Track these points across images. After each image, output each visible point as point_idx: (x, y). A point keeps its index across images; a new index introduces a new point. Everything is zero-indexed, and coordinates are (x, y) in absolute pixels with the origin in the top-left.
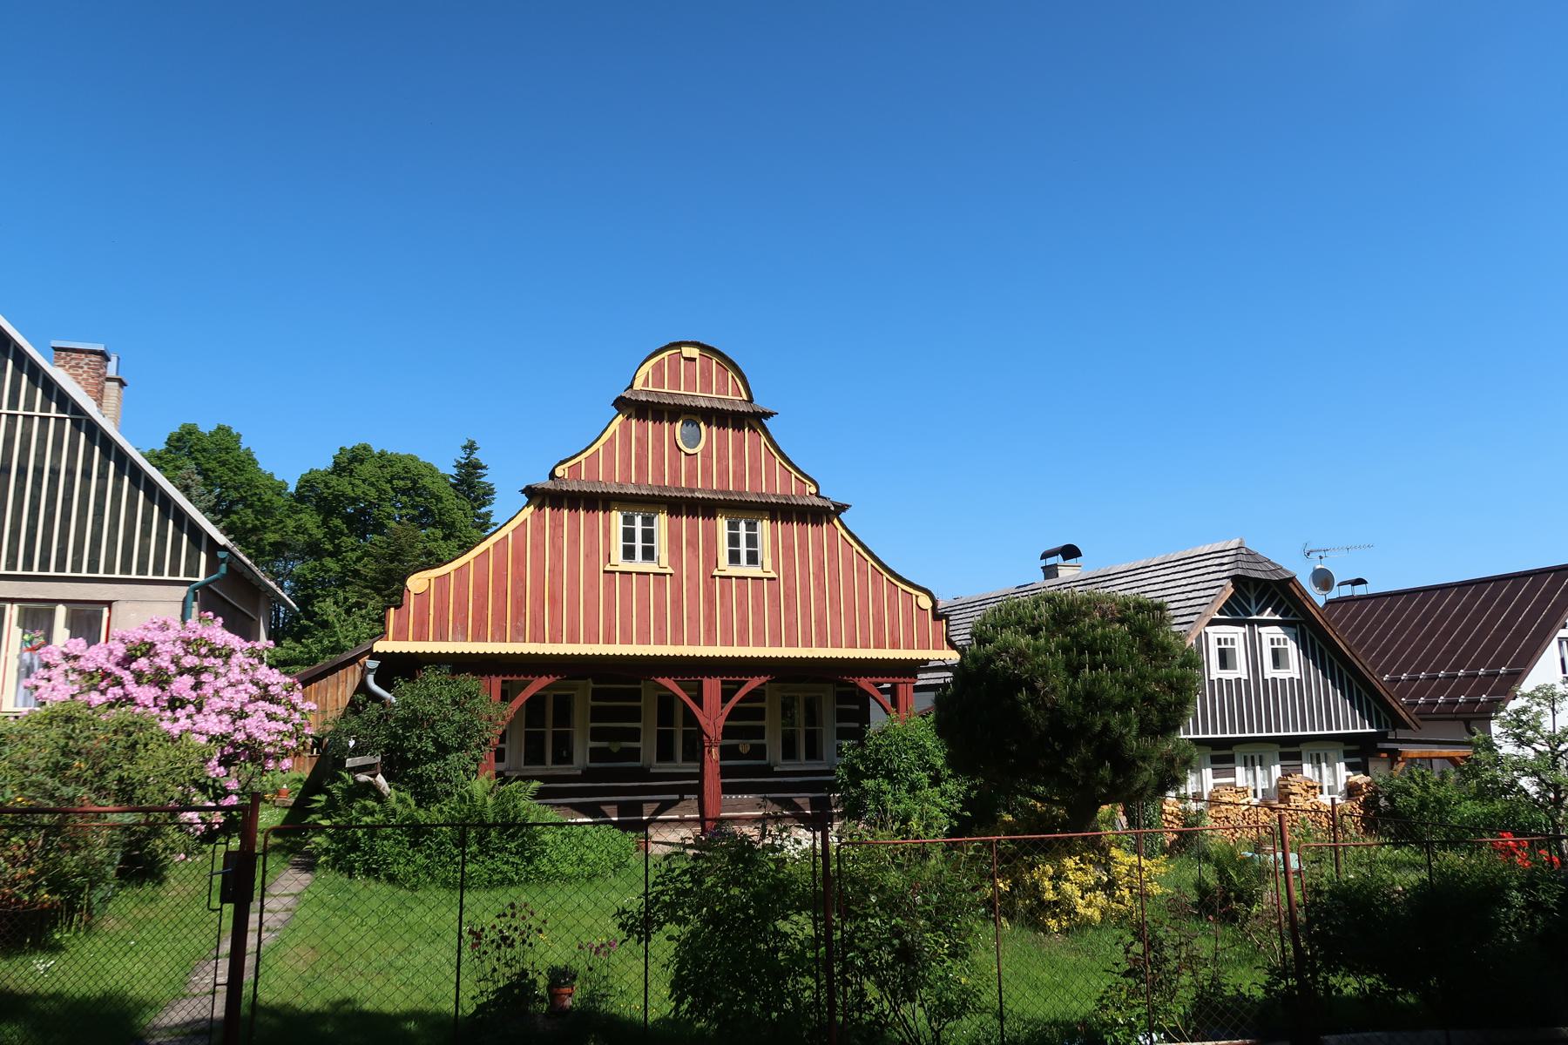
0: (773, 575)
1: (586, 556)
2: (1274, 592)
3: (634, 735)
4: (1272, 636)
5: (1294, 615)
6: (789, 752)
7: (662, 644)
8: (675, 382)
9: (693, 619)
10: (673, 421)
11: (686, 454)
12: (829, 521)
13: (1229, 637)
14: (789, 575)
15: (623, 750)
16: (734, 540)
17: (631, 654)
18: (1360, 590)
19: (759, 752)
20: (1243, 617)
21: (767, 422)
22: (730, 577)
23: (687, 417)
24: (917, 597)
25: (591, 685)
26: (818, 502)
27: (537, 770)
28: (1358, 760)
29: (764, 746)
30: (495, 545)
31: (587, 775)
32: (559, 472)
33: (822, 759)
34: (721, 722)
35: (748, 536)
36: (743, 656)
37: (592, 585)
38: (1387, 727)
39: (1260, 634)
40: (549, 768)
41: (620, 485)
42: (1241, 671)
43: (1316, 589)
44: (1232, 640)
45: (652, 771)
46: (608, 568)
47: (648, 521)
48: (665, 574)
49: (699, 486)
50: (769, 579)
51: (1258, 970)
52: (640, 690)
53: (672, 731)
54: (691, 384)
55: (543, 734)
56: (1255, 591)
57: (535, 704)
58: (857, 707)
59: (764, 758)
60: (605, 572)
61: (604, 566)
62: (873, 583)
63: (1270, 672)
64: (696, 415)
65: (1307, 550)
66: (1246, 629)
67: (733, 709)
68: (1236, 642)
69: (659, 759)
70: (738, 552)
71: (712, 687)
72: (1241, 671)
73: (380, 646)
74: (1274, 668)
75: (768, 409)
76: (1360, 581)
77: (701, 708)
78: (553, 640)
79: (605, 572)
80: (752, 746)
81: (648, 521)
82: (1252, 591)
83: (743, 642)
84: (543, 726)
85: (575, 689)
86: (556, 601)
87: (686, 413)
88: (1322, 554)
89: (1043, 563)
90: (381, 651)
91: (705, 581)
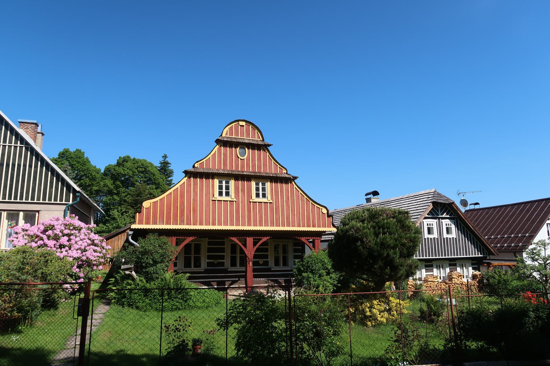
0: (271, 201)
1: (206, 195)
2: (447, 207)
3: (223, 257)
4: (446, 223)
5: (454, 216)
6: (277, 263)
7: (232, 226)
8: (237, 134)
9: (243, 217)
10: (236, 147)
11: (241, 159)
12: (291, 183)
13: (431, 223)
14: (277, 202)
15: (218, 263)
16: (257, 189)
17: (221, 229)
18: (477, 207)
19: (266, 263)
20: (436, 216)
21: (269, 148)
22: (256, 202)
23: (241, 146)
24: (322, 209)
25: (207, 240)
26: (287, 176)
27: (188, 270)
28: (477, 266)
29: (268, 261)
30: (174, 191)
31: (206, 271)
32: (196, 165)
33: (288, 266)
34: (253, 253)
35: (262, 188)
36: (261, 230)
37: (208, 205)
38: (486, 254)
39: (442, 222)
40: (193, 269)
41: (218, 170)
42: (435, 235)
43: (462, 206)
44: (432, 224)
45: (229, 270)
46: (213, 199)
47: (227, 182)
48: (233, 201)
49: (245, 170)
50: (270, 203)
51: (441, 340)
52: (224, 242)
53: (236, 256)
54: (242, 134)
55: (190, 257)
56: (440, 207)
57: (188, 247)
58: (301, 248)
59: (268, 266)
60: (212, 200)
61: (212, 198)
62: (306, 204)
63: (445, 235)
64: (244, 145)
65: (458, 193)
66: (437, 220)
67: (257, 248)
68: (434, 225)
69: (231, 266)
70: (259, 193)
71: (250, 241)
72: (435, 235)
73: (133, 226)
74: (447, 234)
75: (270, 143)
76: (477, 204)
77: (246, 248)
78: (194, 224)
79: (212, 200)
80: (264, 261)
81: (227, 182)
82: (439, 207)
83: (261, 225)
84: (191, 254)
85: (202, 241)
86: (195, 211)
87: (240, 145)
88: (464, 194)
89: (366, 197)
90: (134, 228)
91: (247, 204)
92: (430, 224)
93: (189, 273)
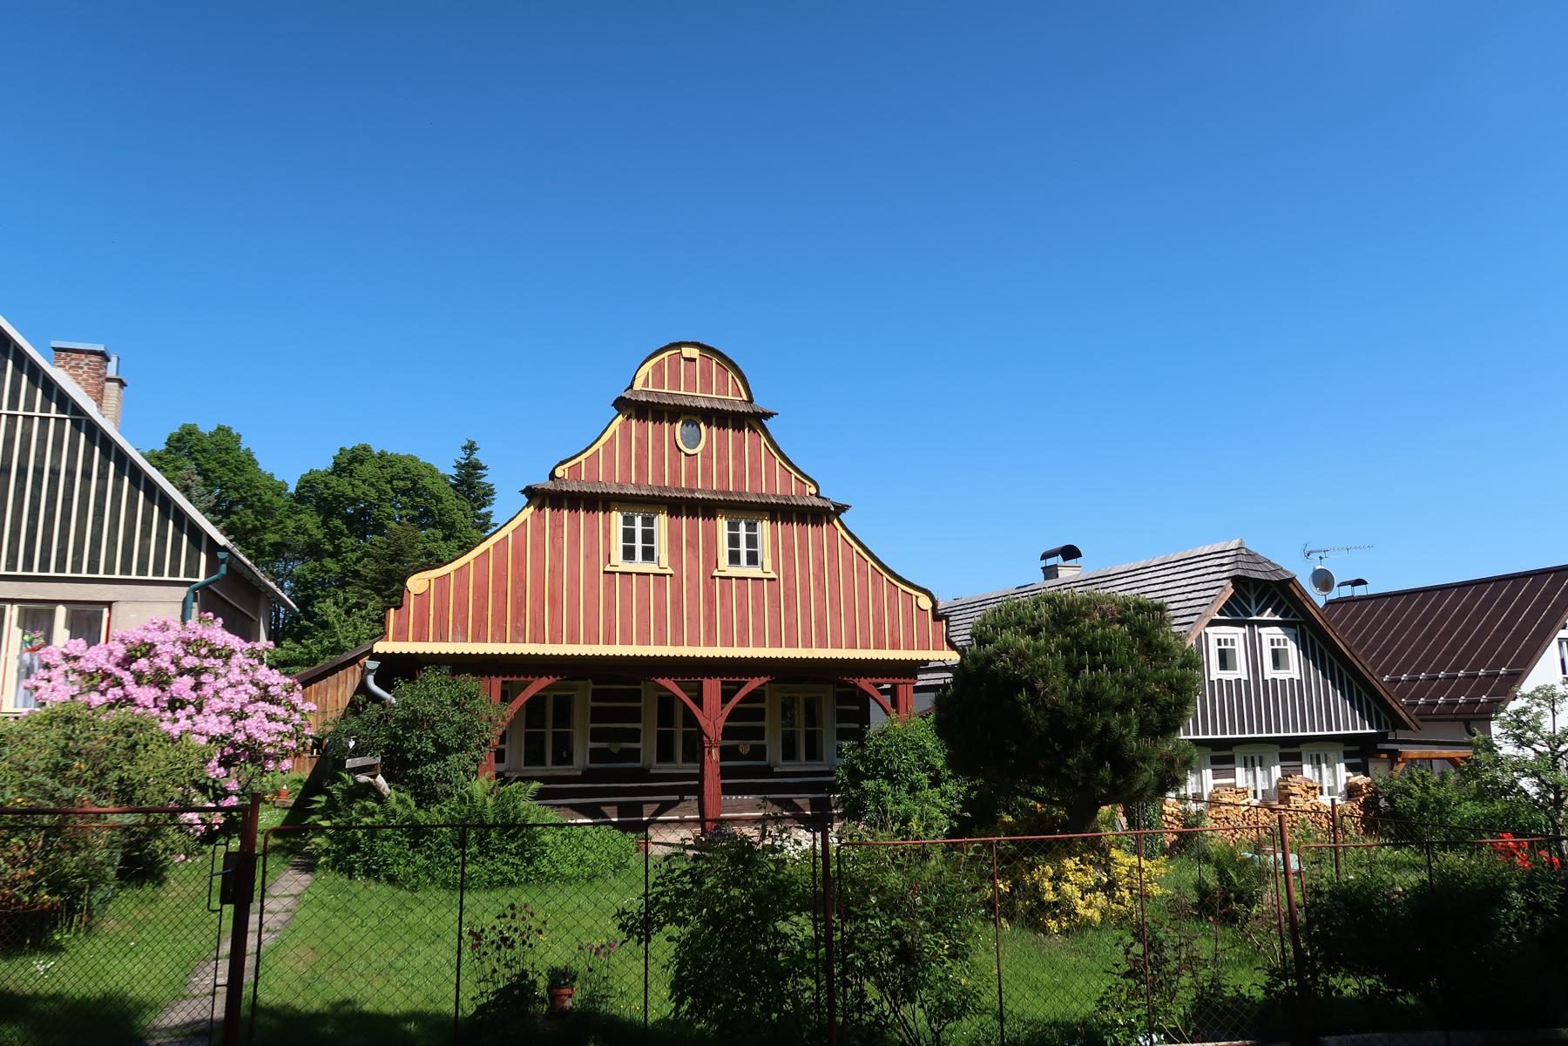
0: (773, 575)
1: (586, 557)
2: (1274, 592)
3: (634, 736)
4: (1272, 637)
5: (1294, 616)
6: (789, 753)
7: (662, 644)
8: (675, 383)
9: (693, 620)
10: (673, 421)
11: (686, 455)
12: (829, 522)
13: (1229, 637)
14: (789, 576)
15: (623, 750)
16: (734, 541)
17: (631, 655)
18: (1360, 591)
19: (759, 753)
20: (1243, 617)
21: (767, 423)
22: (730, 578)
23: (687, 417)
24: (917, 597)
25: (591, 685)
26: (818, 502)
27: (537, 770)
28: (1358, 760)
29: (764, 747)
30: (495, 545)
31: (587, 775)
32: (559, 473)
33: (822, 760)
34: (721, 723)
35: (748, 537)
36: (743, 656)
37: (592, 586)
38: (1387, 727)
39: (1260, 634)
40: (549, 768)
41: (620, 486)
42: (1241, 672)
43: (1316, 590)
44: (1232, 640)
45: (652, 771)
46: (608, 568)
47: (648, 521)
48: (665, 575)
49: (699, 487)
50: (769, 579)
52: (640, 691)
53: (672, 731)
54: (691, 384)
55: (543, 735)
56: (1255, 592)
57: (535, 705)
58: (857, 708)
59: (764, 759)
60: (605, 572)
61: (604, 567)
62: (873, 584)
63: (1270, 673)
64: (696, 415)
65: (1307, 550)
66: (1246, 630)
67: (733, 710)
68: (1236, 643)
69: (659, 760)
70: (738, 552)
71: (712, 687)
72: (1241, 672)
73: (380, 647)
74: (1274, 668)
75: (768, 409)
76: (1360, 582)
77: (701, 708)
78: (553, 641)
79: (605, 572)
80: (752, 747)
81: (648, 521)
82: (1252, 592)
83: (743, 643)
84: (543, 726)
85: (575, 690)
86: (556, 602)
87: (686, 414)
88: (1322, 555)
89: (1043, 563)
90: (381, 652)
91: (705, 582)
92: (1226, 640)
93: (539, 779)
